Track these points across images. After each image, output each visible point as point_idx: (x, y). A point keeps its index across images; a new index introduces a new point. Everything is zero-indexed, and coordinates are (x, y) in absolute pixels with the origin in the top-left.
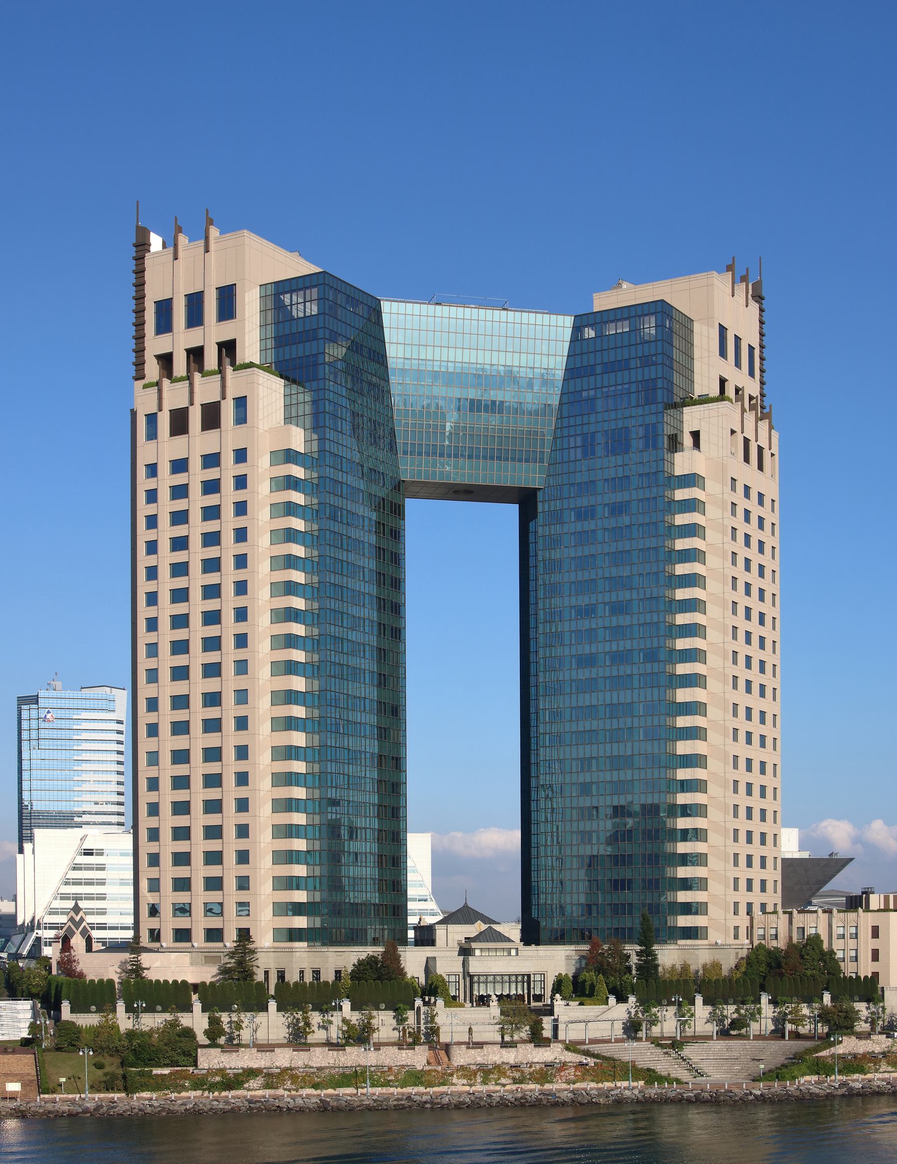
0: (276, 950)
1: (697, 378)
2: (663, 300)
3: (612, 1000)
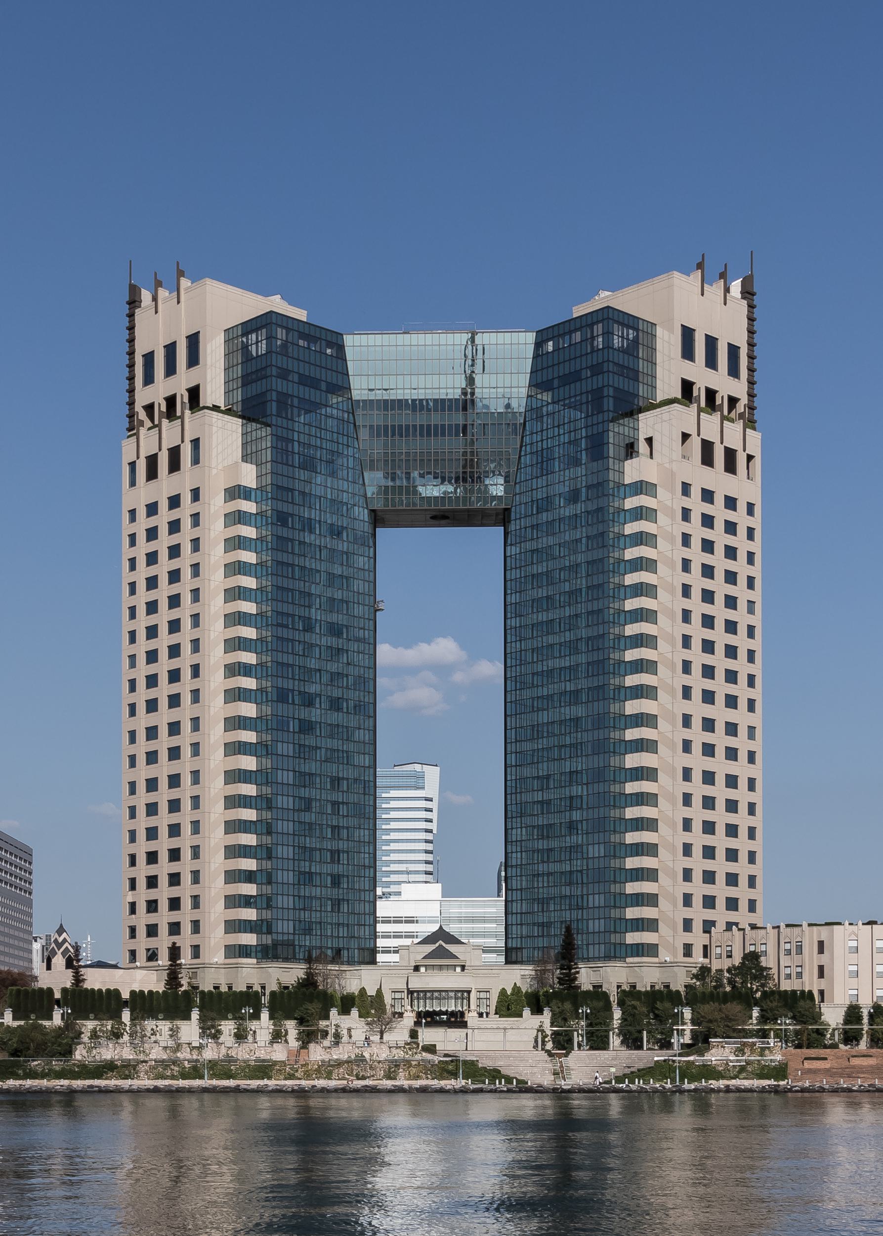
0: (226, 967)
1: (659, 384)
2: (608, 307)
3: (527, 1012)
